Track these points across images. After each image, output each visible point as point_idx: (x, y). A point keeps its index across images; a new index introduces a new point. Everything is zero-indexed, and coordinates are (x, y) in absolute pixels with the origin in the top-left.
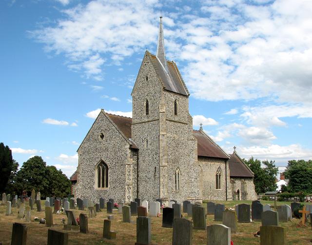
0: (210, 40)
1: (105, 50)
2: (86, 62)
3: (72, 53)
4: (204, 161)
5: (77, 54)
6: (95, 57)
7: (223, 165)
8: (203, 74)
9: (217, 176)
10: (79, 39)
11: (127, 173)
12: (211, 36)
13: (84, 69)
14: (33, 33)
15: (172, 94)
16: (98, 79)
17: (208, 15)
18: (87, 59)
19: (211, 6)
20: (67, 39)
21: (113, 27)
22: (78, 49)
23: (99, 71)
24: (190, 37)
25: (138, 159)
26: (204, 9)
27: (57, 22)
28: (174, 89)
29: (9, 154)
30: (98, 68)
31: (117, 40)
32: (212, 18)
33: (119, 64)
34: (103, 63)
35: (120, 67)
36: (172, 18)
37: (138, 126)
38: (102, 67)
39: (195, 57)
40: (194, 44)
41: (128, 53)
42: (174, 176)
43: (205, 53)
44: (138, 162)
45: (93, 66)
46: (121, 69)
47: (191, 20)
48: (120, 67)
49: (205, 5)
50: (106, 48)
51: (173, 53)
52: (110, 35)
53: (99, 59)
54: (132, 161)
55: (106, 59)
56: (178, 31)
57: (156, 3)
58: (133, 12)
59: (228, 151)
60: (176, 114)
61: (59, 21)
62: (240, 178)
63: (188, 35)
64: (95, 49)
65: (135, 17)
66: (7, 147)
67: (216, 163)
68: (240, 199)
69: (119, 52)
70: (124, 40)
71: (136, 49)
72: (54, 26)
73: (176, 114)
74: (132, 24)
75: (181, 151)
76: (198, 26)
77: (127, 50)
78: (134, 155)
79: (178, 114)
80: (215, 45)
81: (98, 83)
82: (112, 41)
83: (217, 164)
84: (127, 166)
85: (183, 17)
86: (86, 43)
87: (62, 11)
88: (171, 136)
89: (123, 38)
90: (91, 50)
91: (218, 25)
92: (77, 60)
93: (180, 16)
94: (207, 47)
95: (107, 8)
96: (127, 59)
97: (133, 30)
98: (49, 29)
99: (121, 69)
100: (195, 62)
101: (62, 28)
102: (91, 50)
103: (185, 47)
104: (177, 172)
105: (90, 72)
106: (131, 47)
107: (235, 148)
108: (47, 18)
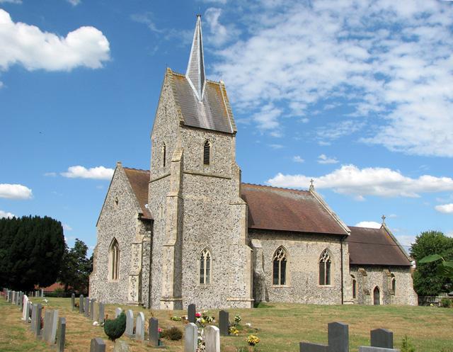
0: (423, 73)
1: (279, 97)
2: (257, 114)
3: (234, 104)
4: (294, 239)
5: (244, 105)
6: (267, 108)
7: (334, 247)
8: (423, 119)
9: (321, 262)
10: (242, 85)
11: (134, 256)
12: (425, 66)
13: (254, 124)
15: (201, 133)
16: (275, 135)
17: (415, 39)
18: (258, 111)
19: (417, 26)
21: (287, 67)
22: (242, 99)
23: (275, 124)
24: (393, 72)
25: (152, 235)
26: (407, 32)
27: (212, 67)
28: (205, 123)
29: (58, 230)
30: (274, 121)
31: (293, 84)
32: (421, 42)
33: (301, 114)
34: (279, 114)
35: (303, 117)
36: (363, 47)
37: (162, 182)
38: (279, 119)
39: (408, 97)
40: (401, 78)
41: (311, 99)
42: (198, 262)
43: (423, 90)
44: (152, 239)
45: (267, 119)
46: (305, 120)
47: (392, 48)
48: (303, 117)
49: (406, 27)
50: (281, 94)
51: (374, 94)
52: (283, 78)
53: (273, 109)
54: (140, 237)
55: (283, 109)
56: (375, 63)
57: (338, 32)
58: (310, 46)
59: (345, 226)
60: (207, 161)
61: (215, 66)
62: (380, 267)
63: (392, 68)
64: (265, 96)
65: (313, 52)
66: (46, 217)
67: (319, 243)
68: (381, 302)
69: (298, 98)
70: (303, 82)
71: (322, 94)
73: (207, 161)
74: (310, 60)
75: (214, 222)
76: (402, 55)
77: (310, 95)
78: (147, 230)
79: (211, 162)
80: (433, 78)
81: (276, 141)
82: (288, 85)
83: (319, 246)
84: (133, 245)
85: (378, 45)
86: (252, 91)
87: (217, 53)
88: (195, 198)
89: (302, 81)
90: (261, 98)
91: (432, 50)
92: (243, 112)
93: (374, 43)
94: (421, 81)
95: (274, 43)
96: (311, 107)
97: (313, 68)
99: (305, 120)
100: (407, 103)
102: (261, 98)
103: (391, 84)
104: (205, 255)
105: (264, 126)
106: (314, 90)
107: (384, 218)
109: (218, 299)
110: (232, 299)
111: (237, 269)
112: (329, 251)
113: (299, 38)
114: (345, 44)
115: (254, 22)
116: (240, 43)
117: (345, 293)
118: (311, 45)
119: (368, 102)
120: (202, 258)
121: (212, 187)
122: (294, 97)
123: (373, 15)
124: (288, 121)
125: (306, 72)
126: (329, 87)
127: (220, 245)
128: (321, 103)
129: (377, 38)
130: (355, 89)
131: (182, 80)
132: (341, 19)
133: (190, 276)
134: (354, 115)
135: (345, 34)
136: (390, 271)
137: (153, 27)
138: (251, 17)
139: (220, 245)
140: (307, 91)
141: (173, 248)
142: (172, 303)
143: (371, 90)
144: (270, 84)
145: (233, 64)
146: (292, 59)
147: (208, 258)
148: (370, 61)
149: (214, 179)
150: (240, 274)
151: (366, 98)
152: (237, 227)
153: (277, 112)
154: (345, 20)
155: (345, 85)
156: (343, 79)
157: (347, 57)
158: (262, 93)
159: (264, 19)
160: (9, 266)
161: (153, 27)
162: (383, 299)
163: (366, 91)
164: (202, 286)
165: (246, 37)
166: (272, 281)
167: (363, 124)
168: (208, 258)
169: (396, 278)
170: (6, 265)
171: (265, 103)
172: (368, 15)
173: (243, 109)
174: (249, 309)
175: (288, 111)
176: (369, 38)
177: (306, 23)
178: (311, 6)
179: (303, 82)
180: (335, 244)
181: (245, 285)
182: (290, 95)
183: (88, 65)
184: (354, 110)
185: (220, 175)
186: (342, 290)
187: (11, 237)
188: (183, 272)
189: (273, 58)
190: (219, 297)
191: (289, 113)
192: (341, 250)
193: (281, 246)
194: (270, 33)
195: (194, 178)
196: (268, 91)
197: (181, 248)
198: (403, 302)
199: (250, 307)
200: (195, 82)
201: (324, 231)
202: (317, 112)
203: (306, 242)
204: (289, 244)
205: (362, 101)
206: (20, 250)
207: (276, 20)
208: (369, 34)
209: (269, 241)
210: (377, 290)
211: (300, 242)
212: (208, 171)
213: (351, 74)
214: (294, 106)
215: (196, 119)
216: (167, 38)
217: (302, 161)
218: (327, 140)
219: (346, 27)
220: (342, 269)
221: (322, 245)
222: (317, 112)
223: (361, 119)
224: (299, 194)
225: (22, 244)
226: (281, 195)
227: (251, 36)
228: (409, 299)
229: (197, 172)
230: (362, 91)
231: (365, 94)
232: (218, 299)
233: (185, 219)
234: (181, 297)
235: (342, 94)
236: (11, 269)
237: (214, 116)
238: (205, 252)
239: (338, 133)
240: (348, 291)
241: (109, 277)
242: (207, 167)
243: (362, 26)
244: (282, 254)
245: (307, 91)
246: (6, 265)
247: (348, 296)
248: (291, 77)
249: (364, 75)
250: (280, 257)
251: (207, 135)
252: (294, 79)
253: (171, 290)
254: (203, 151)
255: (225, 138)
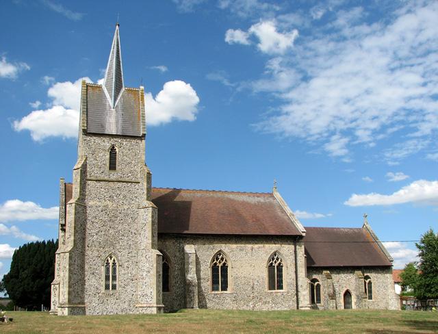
1: (345, 127)
2: (326, 144)
3: (306, 138)
4: (236, 243)
6: (334, 138)
7: (286, 250)
10: (310, 121)
12: (393, 70)
13: (326, 153)
14: (258, 126)
15: (106, 139)
16: (346, 160)
20: (296, 125)
22: (311, 133)
23: (346, 151)
31: (356, 115)
33: (366, 139)
35: (370, 142)
38: (348, 146)
41: (374, 125)
42: (103, 269)
46: (372, 145)
48: (370, 142)
50: (346, 124)
52: (346, 110)
53: (341, 138)
57: (389, 65)
60: (113, 166)
64: (332, 127)
65: (370, 84)
67: (267, 246)
70: (365, 111)
71: (383, 119)
72: (279, 114)
73: (113, 166)
74: (368, 92)
82: (351, 116)
85: (428, 69)
88: (99, 204)
89: (363, 111)
90: (329, 130)
92: (314, 144)
96: (375, 132)
98: (274, 118)
101: (287, 114)
102: (329, 130)
104: (111, 262)
105: (335, 154)
106: (375, 118)
108: (270, 107)
109: (126, 306)
110: (140, 305)
111: (144, 274)
112: (279, 253)
113: (356, 74)
114: (398, 73)
115: (312, 66)
116: (303, 84)
117: (301, 299)
118: (367, 78)
119: (429, 121)
120: (108, 264)
121: (118, 192)
122: (358, 126)
123: (421, 44)
124: (355, 148)
125: (364, 103)
126: (389, 113)
127: (127, 251)
128: (383, 128)
129: (428, 63)
130: (414, 112)
131: (97, 91)
132: (391, 53)
133: (94, 282)
134: (418, 134)
135: (397, 64)
136: (363, 273)
137: (226, 83)
138: (309, 62)
139: (127, 251)
140: (369, 119)
141: (68, 254)
142: (67, 309)
143: (429, 111)
144: (335, 117)
145: (299, 103)
146: (352, 93)
147: (114, 264)
148: (424, 85)
149: (120, 184)
150: (147, 280)
151: (427, 118)
152: (145, 231)
153: (346, 140)
154: (395, 53)
155: (404, 109)
156: (402, 104)
157: (401, 84)
158: (329, 125)
159: (320, 60)
160: (31, 285)
161: (226, 83)
162: (356, 303)
163: (426, 112)
164: (108, 292)
165: (306, 79)
166: (210, 288)
167: (427, 142)
168: (114, 264)
169: (372, 280)
170: (28, 284)
171: (333, 133)
172: (416, 44)
173: (314, 141)
174: (66, 317)
175: (355, 138)
176: (420, 64)
177: (359, 60)
178: (361, 46)
179: (365, 111)
180: (287, 246)
181: (151, 290)
182: (354, 124)
183: (182, 117)
184: (416, 130)
185: (127, 179)
186: (297, 295)
187: (32, 259)
188: (86, 278)
189: (335, 94)
190: (127, 303)
191: (356, 140)
192: (295, 252)
193: (220, 251)
194: (328, 72)
195: (98, 184)
196: (334, 123)
197: (84, 255)
198: (382, 306)
199: (155, 313)
200: (109, 91)
201: (273, 233)
202: (381, 136)
203: (249, 246)
204: (228, 249)
205: (423, 121)
206: (39, 271)
207: (330, 62)
208: (420, 60)
209: (207, 246)
210: (347, 294)
211: (243, 245)
212: (114, 176)
213: (410, 98)
214: (359, 133)
215: (103, 126)
216: (239, 89)
217: (370, 180)
218: (396, 160)
219: (396, 57)
220: (296, 272)
221: (271, 248)
222: (381, 136)
223: (424, 137)
224: (258, 197)
225: (39, 266)
226: (236, 199)
227: (311, 78)
228: (390, 303)
229: (102, 179)
230: (422, 112)
231: (424, 115)
232: (126, 306)
233: (88, 226)
234: (84, 303)
235: (401, 118)
236: (32, 288)
237: (124, 121)
238: (111, 258)
239: (406, 153)
240: (304, 296)
241: (103, 289)
242: (113, 172)
243: (411, 55)
244: (222, 259)
245: (369, 119)
246: (28, 284)
247: (305, 301)
248: (353, 108)
249: (421, 97)
250: (220, 262)
251: (113, 141)
252: (356, 111)
253: (67, 296)
254: (108, 156)
255: (134, 142)
